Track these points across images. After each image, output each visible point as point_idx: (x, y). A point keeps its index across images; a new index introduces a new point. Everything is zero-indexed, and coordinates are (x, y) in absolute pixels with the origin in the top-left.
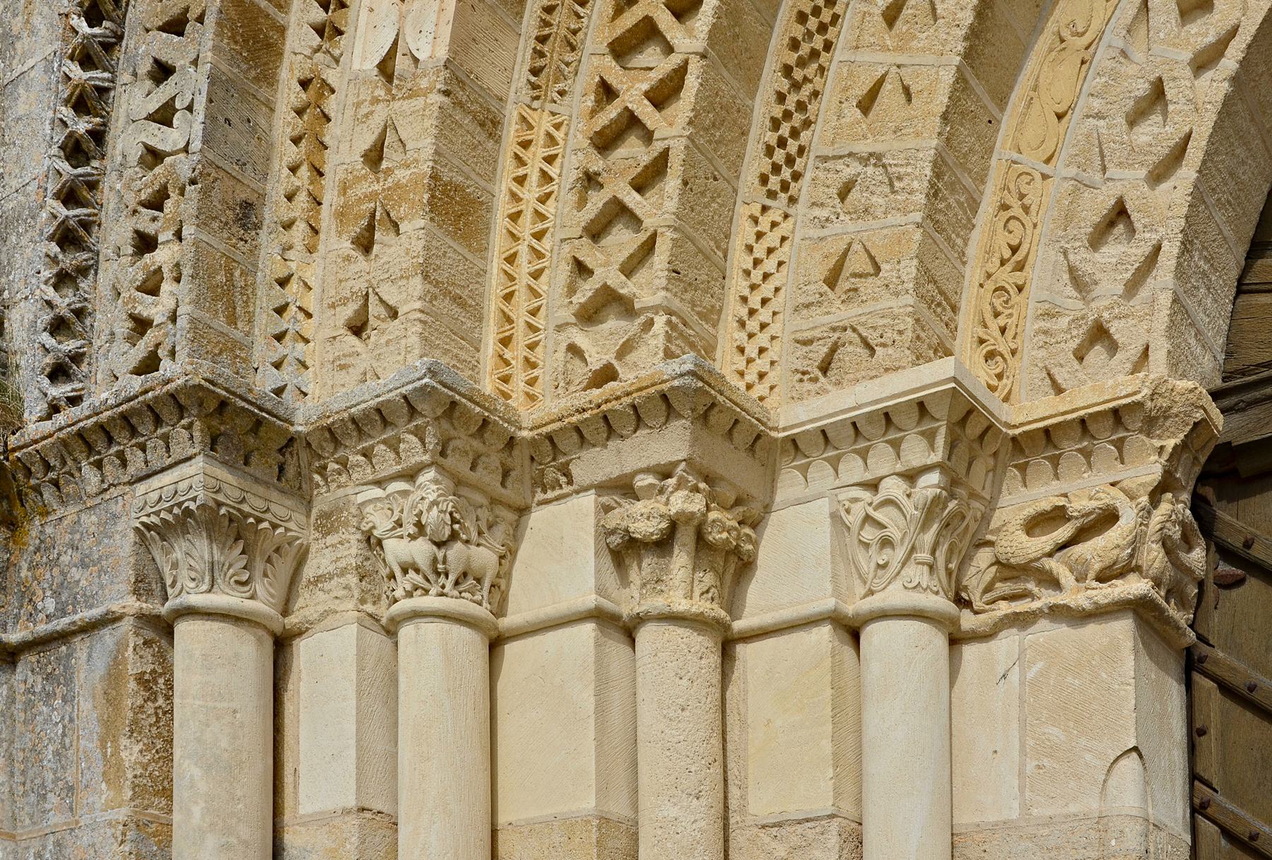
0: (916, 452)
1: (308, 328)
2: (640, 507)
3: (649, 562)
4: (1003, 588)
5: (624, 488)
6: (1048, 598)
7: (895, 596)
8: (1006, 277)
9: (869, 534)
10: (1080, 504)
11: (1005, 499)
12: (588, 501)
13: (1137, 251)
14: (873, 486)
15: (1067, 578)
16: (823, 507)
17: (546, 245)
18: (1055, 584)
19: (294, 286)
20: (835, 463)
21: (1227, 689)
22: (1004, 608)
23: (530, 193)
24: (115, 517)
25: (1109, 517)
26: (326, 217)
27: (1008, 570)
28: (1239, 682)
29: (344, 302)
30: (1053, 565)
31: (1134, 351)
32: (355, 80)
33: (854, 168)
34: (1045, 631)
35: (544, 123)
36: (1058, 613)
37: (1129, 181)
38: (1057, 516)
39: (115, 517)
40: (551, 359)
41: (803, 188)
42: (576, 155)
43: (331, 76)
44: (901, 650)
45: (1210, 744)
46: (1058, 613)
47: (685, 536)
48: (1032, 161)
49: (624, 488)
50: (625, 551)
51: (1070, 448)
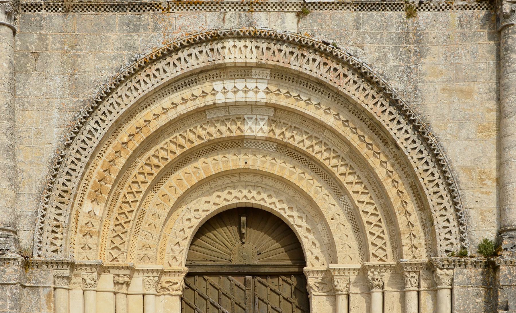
0: (155, 274)
1: (74, 246)
2: (120, 278)
3: (120, 286)
4: (162, 290)
5: (118, 275)
6: (168, 292)
7: (150, 292)
8: (163, 248)
9: (147, 283)
10: (173, 281)
11: (162, 278)
12: (112, 276)
13: (181, 249)
14: (148, 277)
15: (171, 290)
16: (141, 279)
17: (107, 238)
18: (169, 290)
19: (73, 240)
20: (143, 273)
21: (186, 303)
22: (162, 293)
23: (106, 230)
24: (49, 273)
25: (177, 283)
26: (78, 230)
27: (162, 287)
28: (188, 302)
29: (81, 244)
30: (169, 288)
31: (180, 262)
32: (84, 212)
33: (147, 233)
34: (167, 296)
35: (108, 222)
36: (169, 294)
37: (179, 240)
38: (170, 282)
39: (49, 273)
40: (107, 254)
41: (139, 233)
42: (112, 227)
43: (80, 210)
44: (150, 299)
45: (184, 310)
46: (169, 294)
47: (126, 283)
48: (167, 234)
49: (118, 275)
50: (116, 283)
51: (172, 274)
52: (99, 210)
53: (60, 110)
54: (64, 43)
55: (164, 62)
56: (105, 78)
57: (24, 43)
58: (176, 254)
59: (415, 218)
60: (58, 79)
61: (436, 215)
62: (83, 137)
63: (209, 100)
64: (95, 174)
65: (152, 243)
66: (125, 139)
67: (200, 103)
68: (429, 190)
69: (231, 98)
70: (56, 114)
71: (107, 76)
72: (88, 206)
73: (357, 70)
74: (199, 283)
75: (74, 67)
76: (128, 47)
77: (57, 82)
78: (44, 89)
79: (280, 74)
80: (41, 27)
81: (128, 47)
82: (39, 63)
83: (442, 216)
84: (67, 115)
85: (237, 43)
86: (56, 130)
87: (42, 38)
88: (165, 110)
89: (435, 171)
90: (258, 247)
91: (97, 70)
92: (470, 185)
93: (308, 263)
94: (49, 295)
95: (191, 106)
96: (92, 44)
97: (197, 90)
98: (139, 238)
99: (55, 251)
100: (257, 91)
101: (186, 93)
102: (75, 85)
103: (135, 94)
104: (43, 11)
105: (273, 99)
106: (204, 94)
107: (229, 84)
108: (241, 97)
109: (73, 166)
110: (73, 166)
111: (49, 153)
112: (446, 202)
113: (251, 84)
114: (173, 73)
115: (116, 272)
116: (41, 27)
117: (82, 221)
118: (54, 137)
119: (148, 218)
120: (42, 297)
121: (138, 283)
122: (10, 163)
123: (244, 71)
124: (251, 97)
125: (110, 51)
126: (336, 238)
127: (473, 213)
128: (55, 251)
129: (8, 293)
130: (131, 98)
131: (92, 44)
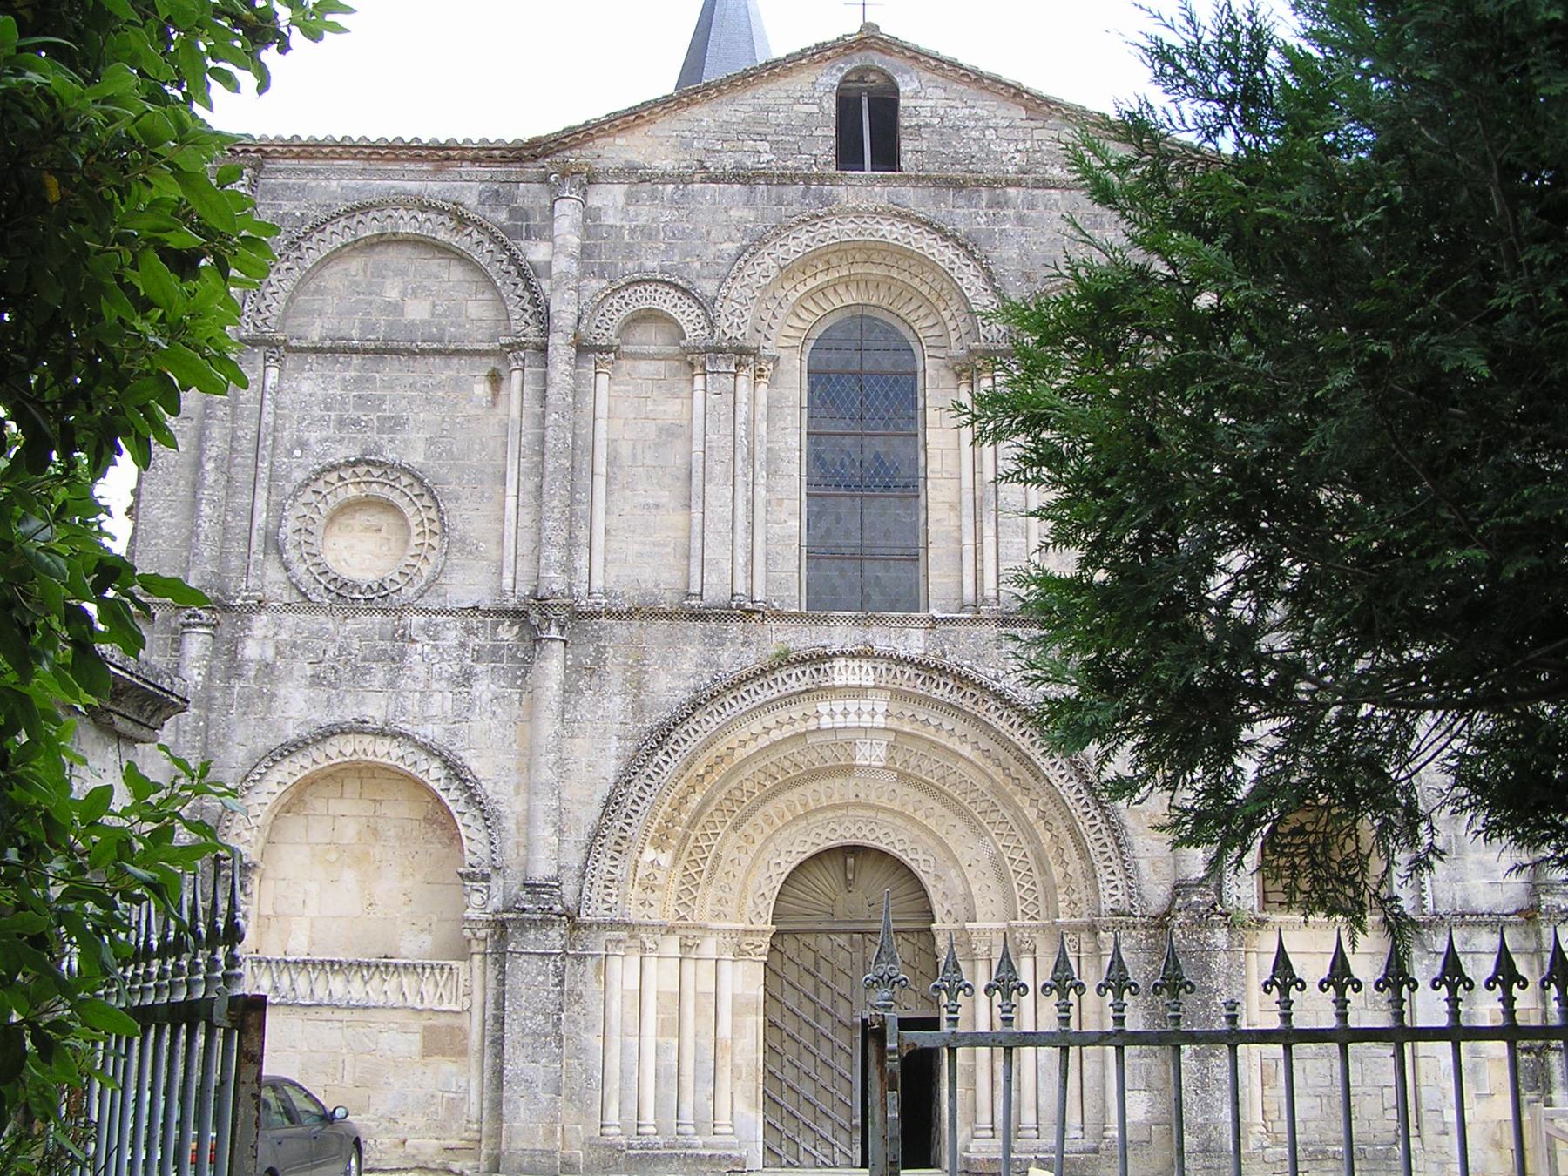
37: (765, 890)
44: (726, 966)
52: (665, 859)
53: (620, 738)
54: (627, 657)
55: (756, 683)
56: (679, 699)
57: (576, 657)
58: (761, 908)
59: (1075, 866)
60: (618, 699)
61: (1099, 866)
62: (648, 771)
63: (812, 724)
64: (660, 814)
65: (729, 896)
66: (701, 772)
67: (800, 727)
68: (1090, 837)
69: (839, 721)
70: (614, 742)
71: (683, 696)
72: (650, 854)
73: (999, 696)
74: (790, 946)
75: (640, 686)
76: (710, 664)
77: (616, 704)
78: (600, 712)
79: (898, 695)
80: (599, 638)
81: (710, 664)
82: (595, 679)
83: (1106, 867)
84: (629, 744)
85: (850, 663)
86: (614, 762)
87: (601, 651)
88: (754, 737)
89: (1096, 813)
90: (870, 895)
91: (669, 689)
92: (1140, 830)
93: (938, 918)
94: (599, 963)
95: (788, 731)
96: (664, 659)
97: (796, 711)
98: (711, 890)
99: (609, 909)
100: (873, 714)
101: (782, 714)
102: (639, 709)
103: (718, 719)
104: (603, 619)
105: (894, 723)
106: (805, 718)
107: (838, 706)
108: (852, 721)
109: (635, 807)
110: (635, 807)
111: (603, 791)
112: (1110, 850)
113: (866, 706)
114: (766, 695)
115: (685, 932)
116: (599, 638)
117: (641, 873)
118: (610, 768)
119: (724, 865)
120: (589, 968)
121: (709, 947)
122: (555, 803)
123: (859, 692)
124: (866, 721)
125: (687, 667)
126: (974, 889)
127: (1143, 864)
128: (609, 909)
129: (551, 966)
130: (713, 723)
131: (664, 659)
